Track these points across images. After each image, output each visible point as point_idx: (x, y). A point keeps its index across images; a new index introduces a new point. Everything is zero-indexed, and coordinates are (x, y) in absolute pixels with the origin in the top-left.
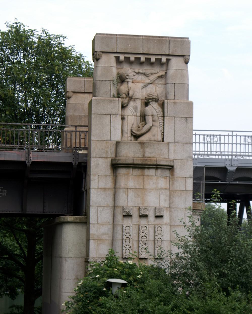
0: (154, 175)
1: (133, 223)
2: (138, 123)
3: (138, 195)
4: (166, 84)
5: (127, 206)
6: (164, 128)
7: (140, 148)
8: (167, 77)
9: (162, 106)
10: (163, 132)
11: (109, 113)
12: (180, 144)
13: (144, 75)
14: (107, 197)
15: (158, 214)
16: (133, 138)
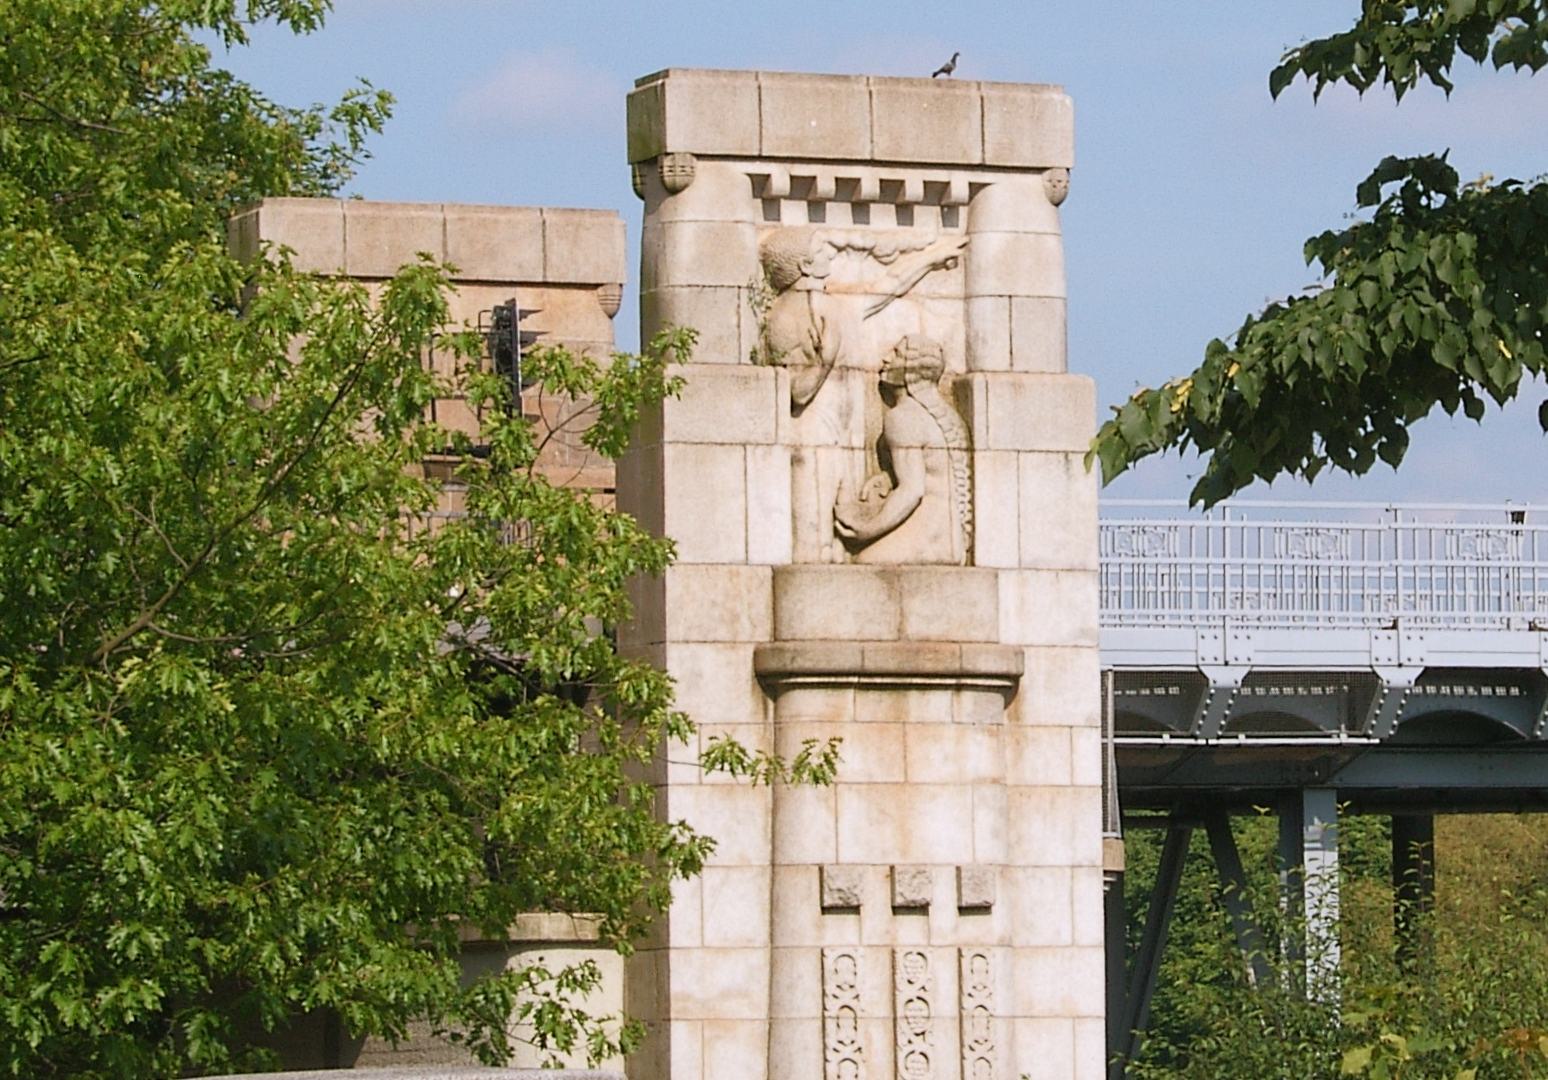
0: (949, 719)
1: (865, 942)
3: (882, 812)
4: (967, 298)
5: (837, 864)
6: (972, 502)
7: (883, 597)
9: (962, 394)
10: (972, 522)
11: (741, 438)
12: (1044, 574)
14: (739, 823)
15: (970, 899)
16: (839, 545)
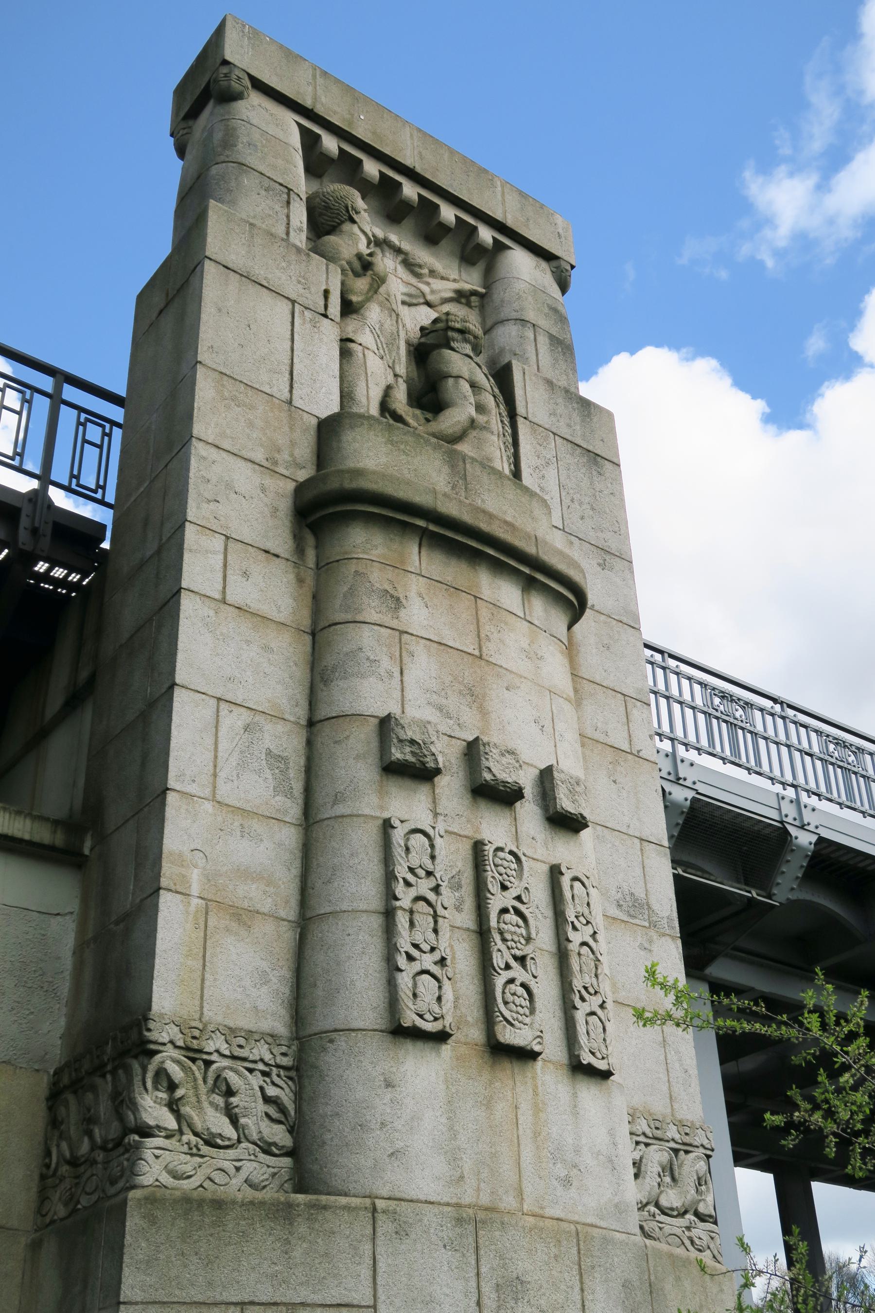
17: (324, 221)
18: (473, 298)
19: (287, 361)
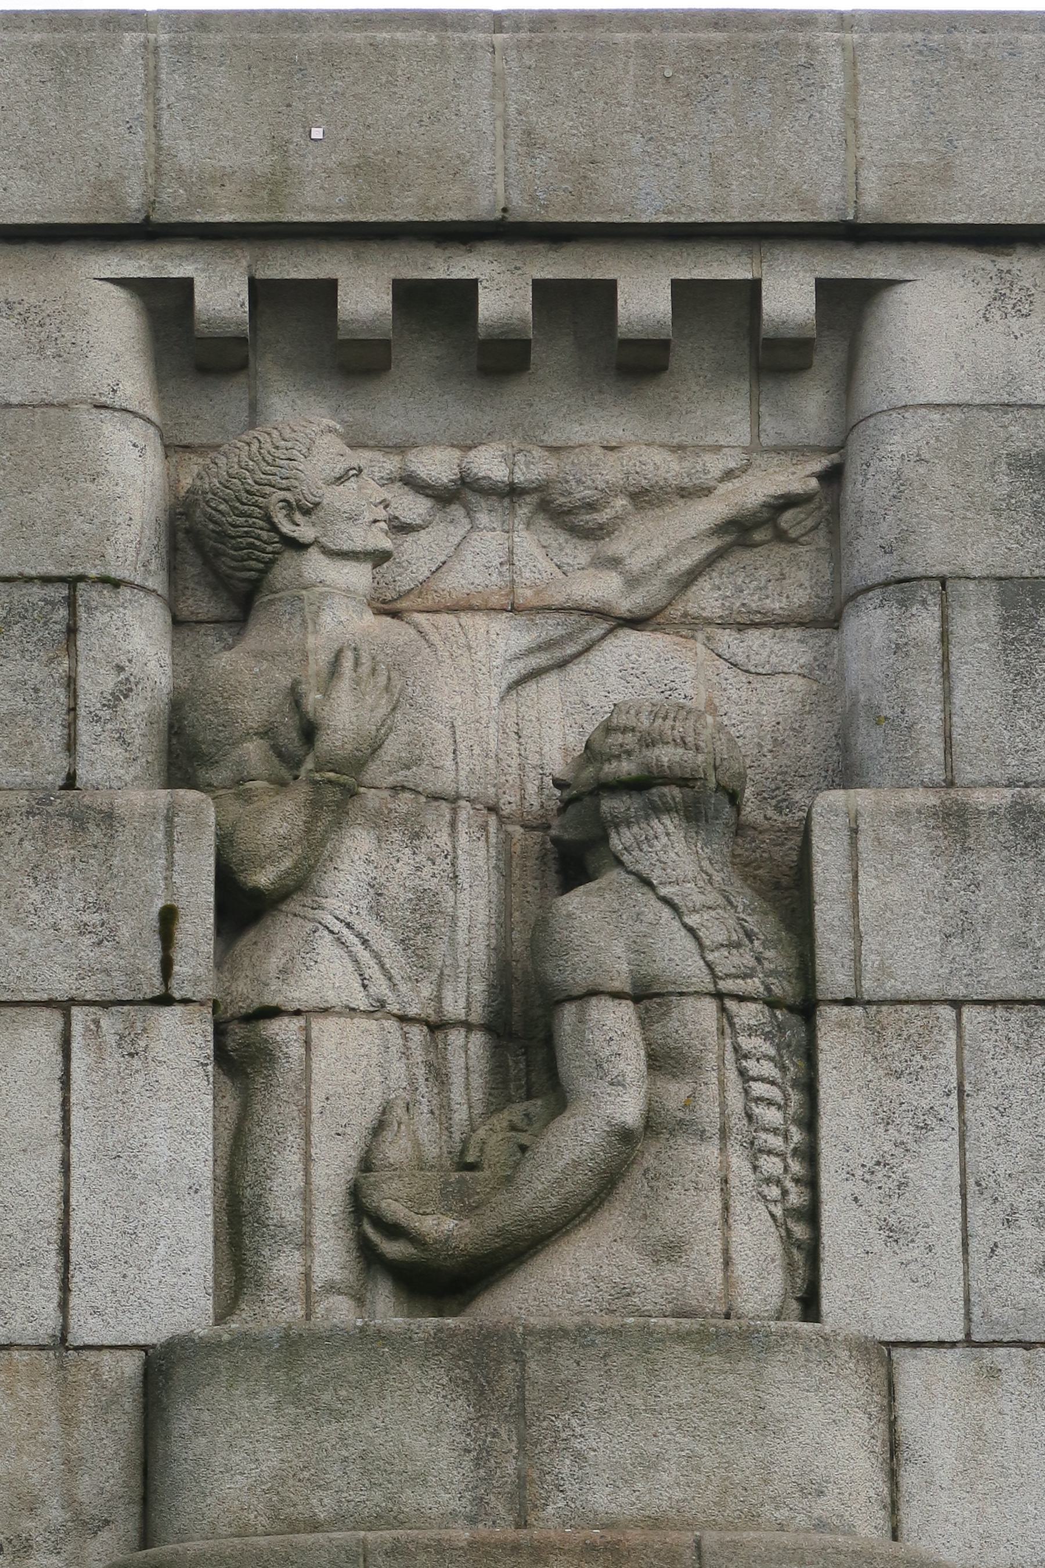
2: (460, 1115)
8: (848, 521)
10: (811, 1215)
13: (541, 521)
17: (229, 571)
18: (787, 519)
19: (51, 1215)
